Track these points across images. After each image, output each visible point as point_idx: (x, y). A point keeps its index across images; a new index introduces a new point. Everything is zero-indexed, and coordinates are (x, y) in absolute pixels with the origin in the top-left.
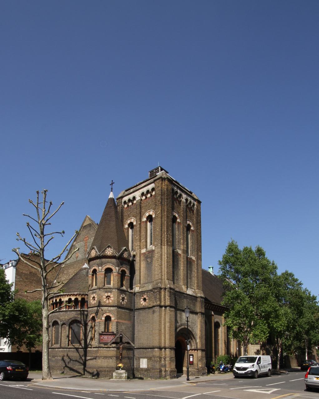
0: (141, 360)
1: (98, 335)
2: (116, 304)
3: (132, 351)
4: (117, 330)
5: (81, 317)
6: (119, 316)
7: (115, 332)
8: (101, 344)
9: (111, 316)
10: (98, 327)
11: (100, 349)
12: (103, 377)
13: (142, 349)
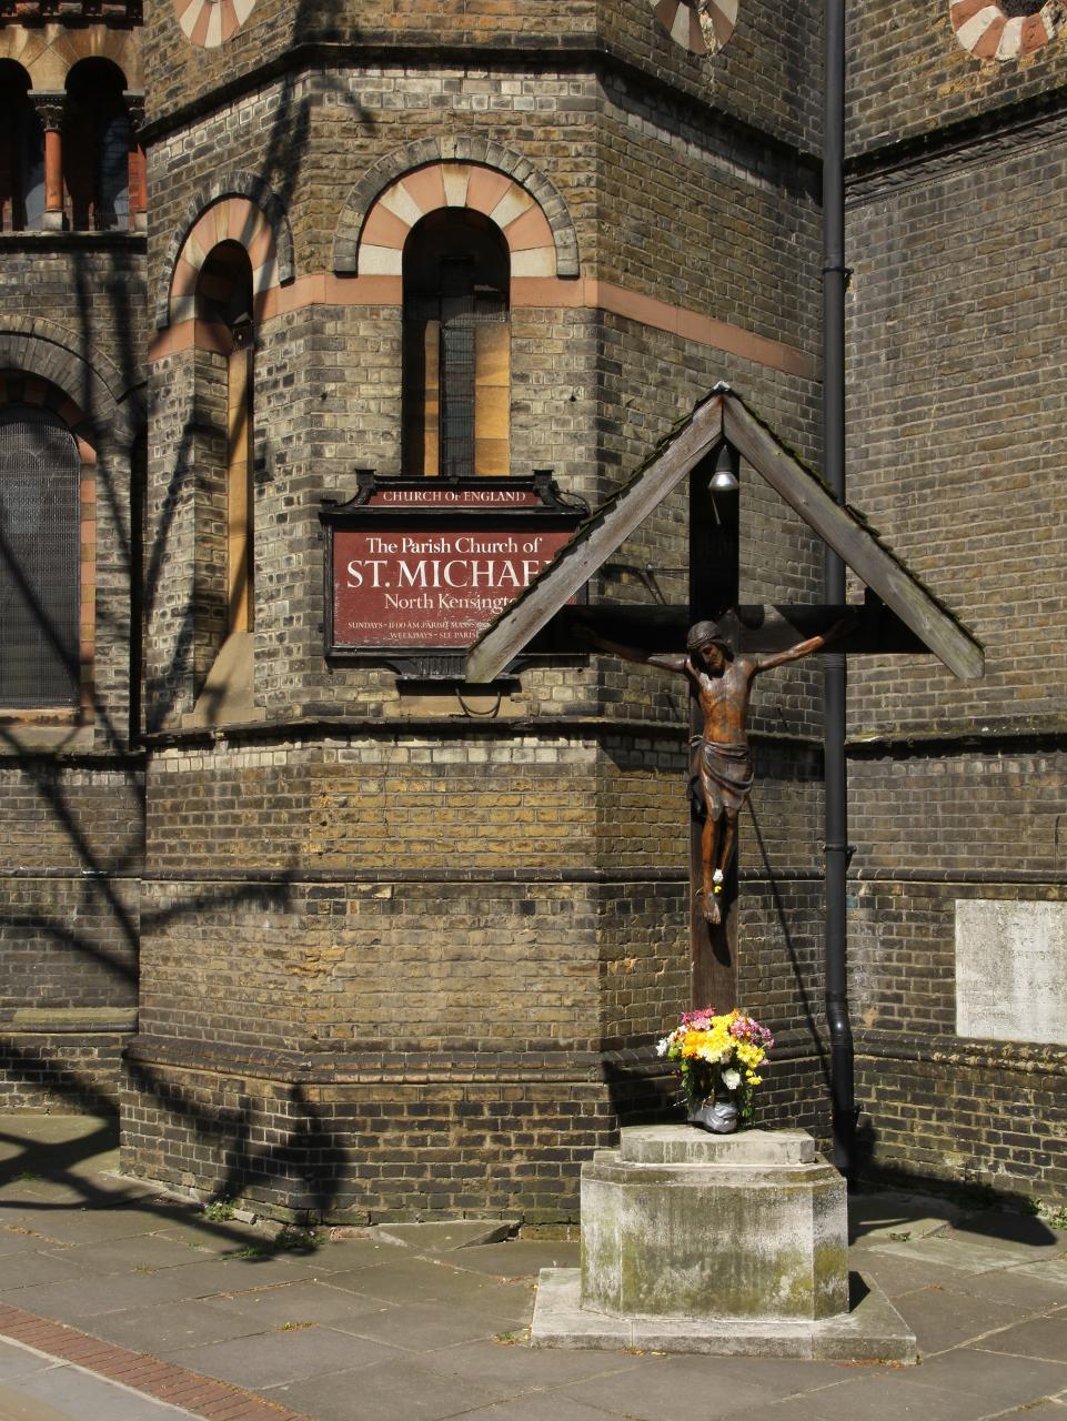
0: (972, 920)
1: (300, 530)
2: (587, 26)
3: (815, 789)
4: (611, 442)
5: (87, 334)
6: (627, 222)
7: (576, 485)
8: (356, 676)
9: (504, 211)
10: (299, 408)
11: (334, 751)
12: (398, 1212)
13: (988, 746)
